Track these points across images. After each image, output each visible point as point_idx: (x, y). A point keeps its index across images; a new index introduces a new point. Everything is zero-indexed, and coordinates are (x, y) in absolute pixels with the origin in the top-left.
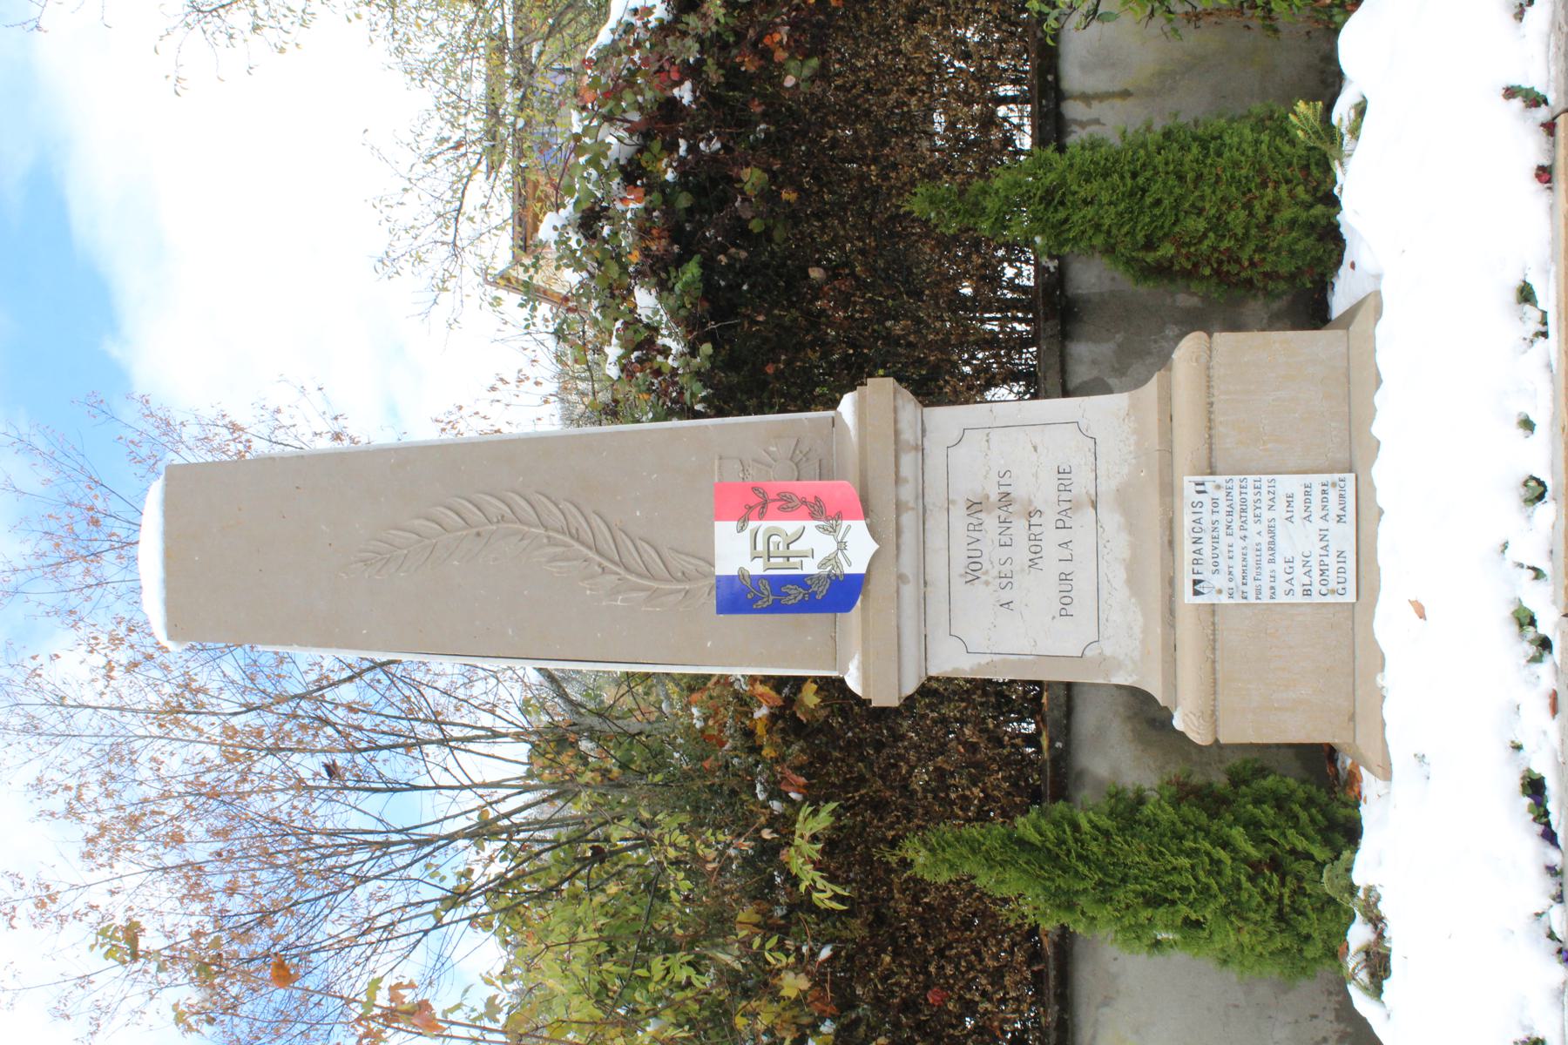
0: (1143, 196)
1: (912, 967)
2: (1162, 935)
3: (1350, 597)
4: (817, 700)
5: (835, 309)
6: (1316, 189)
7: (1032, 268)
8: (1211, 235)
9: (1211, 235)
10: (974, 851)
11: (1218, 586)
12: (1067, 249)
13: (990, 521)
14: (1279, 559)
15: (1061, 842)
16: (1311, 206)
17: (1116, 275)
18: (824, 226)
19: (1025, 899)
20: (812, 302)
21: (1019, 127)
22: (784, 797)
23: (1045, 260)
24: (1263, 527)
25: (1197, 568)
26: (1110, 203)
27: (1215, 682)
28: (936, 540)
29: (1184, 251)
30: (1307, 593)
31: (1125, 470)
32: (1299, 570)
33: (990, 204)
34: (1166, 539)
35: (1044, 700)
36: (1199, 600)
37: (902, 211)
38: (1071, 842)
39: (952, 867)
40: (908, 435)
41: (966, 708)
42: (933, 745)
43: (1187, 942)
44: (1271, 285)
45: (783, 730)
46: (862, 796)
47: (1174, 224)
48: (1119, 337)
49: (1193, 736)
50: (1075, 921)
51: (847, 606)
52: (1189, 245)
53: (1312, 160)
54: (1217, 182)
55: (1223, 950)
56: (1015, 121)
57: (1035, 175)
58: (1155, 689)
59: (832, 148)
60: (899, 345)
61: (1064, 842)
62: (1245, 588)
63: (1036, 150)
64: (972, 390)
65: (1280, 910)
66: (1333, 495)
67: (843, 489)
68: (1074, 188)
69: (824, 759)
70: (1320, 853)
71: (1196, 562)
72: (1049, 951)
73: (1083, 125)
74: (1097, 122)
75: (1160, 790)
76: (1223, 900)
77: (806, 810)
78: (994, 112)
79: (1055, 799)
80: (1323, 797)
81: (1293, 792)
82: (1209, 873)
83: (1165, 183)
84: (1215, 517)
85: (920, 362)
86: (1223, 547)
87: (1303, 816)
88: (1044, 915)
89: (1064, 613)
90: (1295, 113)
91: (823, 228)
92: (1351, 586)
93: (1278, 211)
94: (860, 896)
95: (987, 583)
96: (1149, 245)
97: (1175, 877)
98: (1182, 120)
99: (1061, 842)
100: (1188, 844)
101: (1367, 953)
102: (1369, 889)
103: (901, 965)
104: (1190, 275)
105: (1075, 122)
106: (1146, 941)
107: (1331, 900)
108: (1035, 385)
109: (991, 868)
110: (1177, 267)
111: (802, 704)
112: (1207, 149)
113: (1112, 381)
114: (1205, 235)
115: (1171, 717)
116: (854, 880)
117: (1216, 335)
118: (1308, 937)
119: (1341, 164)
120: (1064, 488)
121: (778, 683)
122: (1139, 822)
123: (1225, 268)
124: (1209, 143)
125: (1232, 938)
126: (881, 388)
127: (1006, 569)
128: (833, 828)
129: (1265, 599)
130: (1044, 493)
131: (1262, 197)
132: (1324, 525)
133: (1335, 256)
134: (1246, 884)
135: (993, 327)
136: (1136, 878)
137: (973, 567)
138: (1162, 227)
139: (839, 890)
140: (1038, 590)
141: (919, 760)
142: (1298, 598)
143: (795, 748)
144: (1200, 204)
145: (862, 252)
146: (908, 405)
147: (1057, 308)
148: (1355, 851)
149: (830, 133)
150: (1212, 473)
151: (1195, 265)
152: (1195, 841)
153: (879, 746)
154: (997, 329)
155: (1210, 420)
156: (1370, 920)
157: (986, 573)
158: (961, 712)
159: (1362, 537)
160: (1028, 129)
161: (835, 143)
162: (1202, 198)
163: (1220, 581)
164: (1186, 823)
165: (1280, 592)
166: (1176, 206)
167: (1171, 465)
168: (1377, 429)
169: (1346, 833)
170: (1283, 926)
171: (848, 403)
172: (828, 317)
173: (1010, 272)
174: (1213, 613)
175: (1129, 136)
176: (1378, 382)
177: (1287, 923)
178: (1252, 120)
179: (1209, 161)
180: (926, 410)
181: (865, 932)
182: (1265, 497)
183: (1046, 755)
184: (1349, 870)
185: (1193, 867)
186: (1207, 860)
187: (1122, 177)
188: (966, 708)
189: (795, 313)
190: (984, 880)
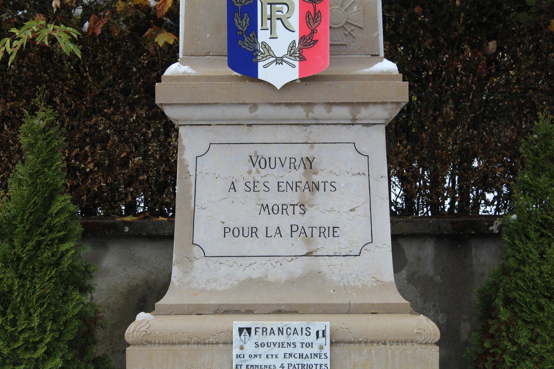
0: (546, 297)
4: (161, 44)
5: (464, 61)
7: (493, 213)
8: (515, 348)
9: (515, 348)
10: (43, 162)
11: (245, 346)
12: (506, 238)
13: (297, 175)
15: (51, 229)
18: (529, 53)
20: (469, 43)
22: (85, 17)
23: (498, 222)
25: (260, 330)
26: (541, 272)
27: (173, 344)
28: (283, 134)
29: (503, 327)
31: (335, 278)
34: (283, 308)
35: (161, 218)
36: (236, 332)
37: (539, 113)
38: (51, 236)
39: (31, 145)
40: (364, 113)
41: (155, 159)
42: (126, 134)
45: (137, 17)
46: (87, 78)
47: (524, 320)
48: (438, 278)
49: (132, 327)
51: (232, 65)
52: (508, 331)
58: (168, 300)
60: (435, 110)
61: (51, 231)
64: (400, 162)
67: (325, 65)
69: (116, 49)
71: (264, 330)
77: (75, 33)
79: (84, 225)
82: (26, 341)
84: (298, 345)
85: (421, 128)
86: (275, 350)
91: (527, 52)
94: (8, 76)
95: (250, 172)
96: (508, 301)
97: (23, 315)
99: (51, 229)
100: (49, 325)
104: (485, 333)
108: (400, 216)
109: (31, 175)
110: (490, 322)
111: (159, 32)
113: (404, 273)
114: (515, 344)
115: (146, 312)
116: (21, 72)
120: (322, 231)
121: (174, 14)
122: (66, 289)
126: (401, 92)
127: (260, 187)
128: (62, 54)
130: (318, 217)
136: (23, 286)
137: (263, 162)
138: (522, 311)
139: (12, 58)
141: (115, 122)
143: (124, 27)
144: (539, 340)
145: (508, 82)
146: (385, 114)
147: (462, 232)
150: (331, 343)
151: (492, 336)
152: (52, 331)
153: (126, 92)
154: (446, 185)
155: (372, 342)
157: (258, 172)
158: (152, 155)
162: (544, 342)
163: (250, 348)
164: (66, 323)
166: (538, 323)
171: (389, 66)
172: (458, 55)
173: (490, 197)
180: (383, 127)
183: (119, 219)
185: (32, 329)
188: (155, 159)
189: (461, 30)
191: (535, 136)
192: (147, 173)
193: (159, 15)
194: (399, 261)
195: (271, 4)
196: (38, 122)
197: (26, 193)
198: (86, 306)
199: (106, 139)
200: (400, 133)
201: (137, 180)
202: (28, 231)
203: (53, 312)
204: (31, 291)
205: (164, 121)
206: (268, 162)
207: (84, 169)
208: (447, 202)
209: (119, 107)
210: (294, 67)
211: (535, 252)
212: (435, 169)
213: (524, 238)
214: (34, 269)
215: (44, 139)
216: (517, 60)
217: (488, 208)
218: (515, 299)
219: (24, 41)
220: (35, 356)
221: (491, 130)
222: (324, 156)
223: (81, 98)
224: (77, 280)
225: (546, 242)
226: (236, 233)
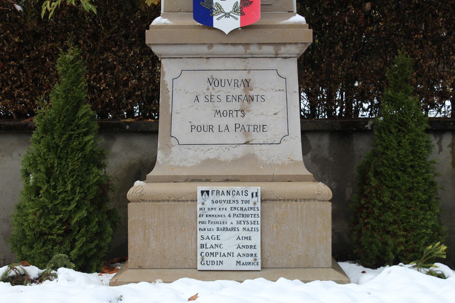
0: (401, 170)
1: (13, 53)
2: (31, 177)
3: (200, 267)
5: (349, 16)
6: (402, 255)
7: (367, 116)
8: (381, 204)
9: (381, 204)
10: (73, 83)
11: (205, 203)
12: (376, 133)
13: (239, 91)
14: (219, 233)
15: (78, 126)
16: (394, 253)
17: (362, 158)
19: (48, 109)
21: (439, 111)
23: (371, 123)
24: (235, 225)
25: (215, 192)
26: (398, 154)
27: (159, 201)
28: (230, 64)
29: (373, 190)
30: (202, 246)
31: (264, 159)
32: (213, 242)
33: (400, 94)
34: (230, 178)
35: (150, 120)
36: (199, 194)
37: (399, 51)
38: (78, 131)
39: (64, 72)
40: (283, 50)
41: (146, 81)
42: (127, 64)
43: (28, 188)
44: (355, 233)
46: (100, 27)
47: (387, 186)
48: (331, 159)
49: (131, 190)
50: (38, 133)
51: (196, 18)
52: (376, 193)
53: (417, 254)
54: (407, 207)
55: (25, 206)
56: (443, 109)
57: (414, 117)
58: (154, 173)
59: (433, 15)
60: (330, 49)
61: (78, 128)
62: (205, 216)
63: (426, 119)
65: (45, 234)
66: (250, 259)
67: (257, 18)
68: (407, 137)
70: (74, 252)
71: (218, 192)
72: (23, 122)
73: (439, 143)
74: (441, 150)
75: (106, 176)
76: (50, 206)
78: (447, 99)
79: (100, 124)
80: (102, 255)
81: (104, 240)
82: (63, 199)
83: (408, 182)
86: (225, 205)
87: (92, 245)
88: (41, 118)
89: (192, 128)
90: (440, 244)
91: (391, 10)
92: (205, 267)
93: (392, 237)
94: (48, 26)
95: (208, 89)
96: (377, 174)
97: (61, 182)
98: (440, 191)
99: (78, 126)
100: (78, 189)
101: (24, 275)
102: (56, 276)
103: (13, 47)
104: (362, 194)
105: (441, 139)
106: (28, 168)
107: (50, 258)
109: (64, 91)
110: (365, 187)
112: (425, 203)
113: (309, 155)
114: (381, 201)
115: (141, 180)
116: (57, 23)
117: (331, 204)
118: (32, 248)
119: (414, 267)
120: (256, 128)
122: (88, 166)
123: (364, 211)
124: (427, 204)
125: (31, 211)
126: (307, 36)
127: (215, 99)
128: (84, 12)
129: (199, 226)
131: (399, 229)
132: (236, 255)
133: (369, 264)
134: (58, 218)
135: (338, 96)
136: (60, 164)
137: (216, 82)
138: (386, 180)
139: (51, 14)
140: (204, 115)
141: (120, 57)
142: (200, 242)
144: (396, 199)
145: (378, 30)
147: (347, 129)
148: (75, 269)
149: (440, 14)
150: (262, 201)
151: (366, 196)
152: (79, 193)
153: (126, 37)
154: (337, 98)
155: (288, 200)
156: (40, 276)
157: (213, 89)
159: (230, 273)
160: (439, 115)
161: (435, 16)
162: (400, 200)
163: (208, 204)
164: (88, 188)
165: (202, 233)
167: (266, 181)
168: (282, 280)
169: (84, 266)
170: (38, 235)
171: (299, 19)
172: (345, 12)
173: (366, 106)
174: (192, 201)
175: (432, 165)
176: (305, 282)
177: (39, 238)
178: (438, 225)
179: (418, 203)
180: (296, 59)
181: (30, 29)
182: (250, 226)
184: (65, 266)
185: (67, 191)
186: (70, 198)
187: (411, 161)
190: (58, 88)
191: (396, 65)
196: (69, 57)
197: (61, 103)
201: (134, 95)
202: (63, 128)
203: (80, 181)
204: (66, 167)
205: (152, 56)
206: (220, 82)
207: (100, 87)
209: (122, 47)
210: (237, 19)
211: (395, 141)
212: (330, 88)
213: (387, 133)
214: (67, 152)
215: (73, 68)
217: (365, 113)
218: (381, 172)
220: (69, 209)
222: (257, 79)
224: (96, 160)
225: (402, 135)
226: (199, 129)
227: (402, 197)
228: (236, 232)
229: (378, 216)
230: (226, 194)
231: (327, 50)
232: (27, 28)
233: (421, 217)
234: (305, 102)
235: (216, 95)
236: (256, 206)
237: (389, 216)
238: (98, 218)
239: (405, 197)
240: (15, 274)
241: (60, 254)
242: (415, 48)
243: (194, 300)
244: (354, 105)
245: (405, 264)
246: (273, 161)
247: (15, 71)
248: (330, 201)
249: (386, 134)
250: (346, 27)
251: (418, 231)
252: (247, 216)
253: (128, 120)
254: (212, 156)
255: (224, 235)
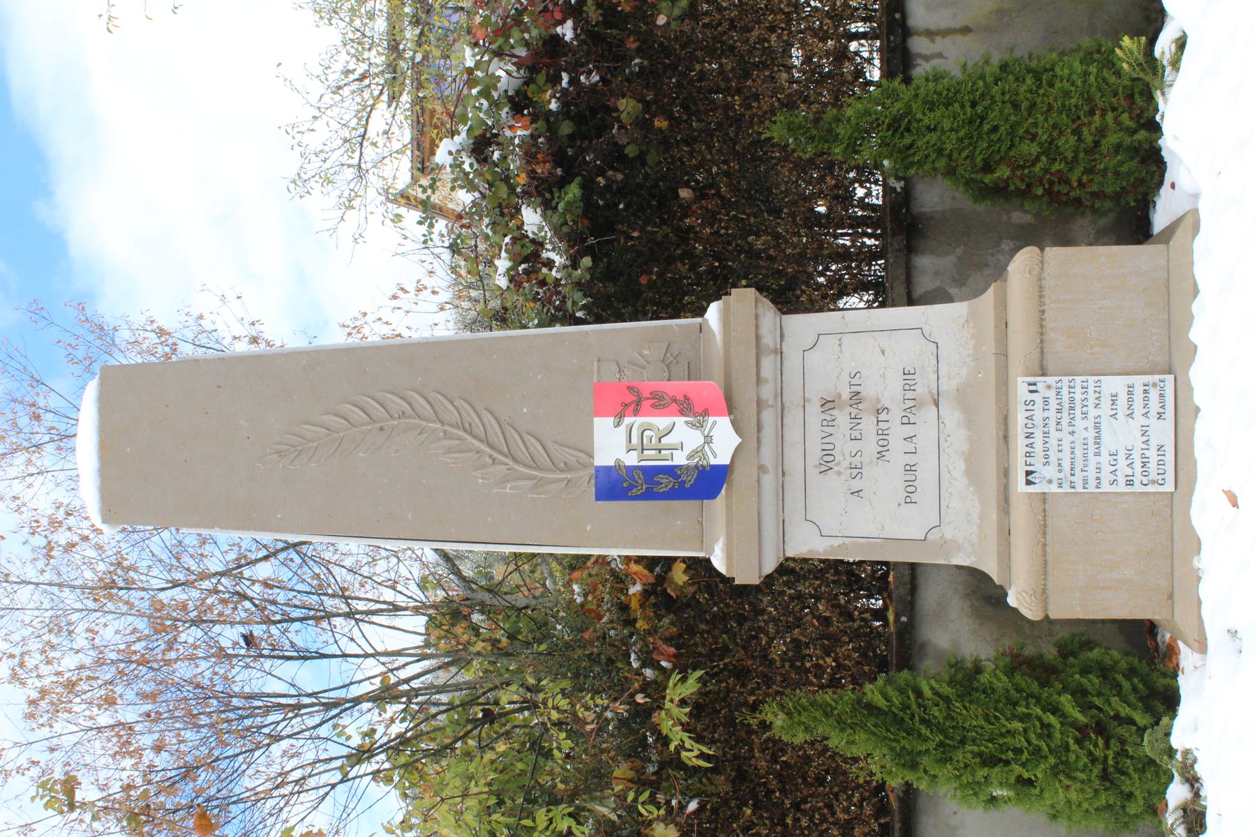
0: (981, 123)
2: (998, 792)
3: (1169, 487)
4: (685, 578)
6: (1139, 116)
7: (880, 188)
8: (1044, 158)
9: (1044, 158)
10: (826, 715)
11: (1048, 477)
12: (912, 171)
13: (842, 418)
15: (905, 707)
16: (1135, 132)
18: (693, 151)
19: (874, 759)
20: (681, 219)
21: (869, 61)
22: (656, 666)
23: (892, 182)
24: (1090, 424)
25: (1029, 460)
26: (952, 130)
27: (1045, 562)
28: (793, 435)
29: (1019, 173)
30: (1130, 483)
31: (964, 372)
32: (1122, 463)
34: (1001, 434)
35: (891, 579)
36: (1031, 489)
37: (763, 137)
38: (914, 707)
40: (768, 340)
41: (820, 586)
42: (791, 619)
44: (1098, 204)
45: (654, 605)
46: (726, 665)
47: (1010, 148)
48: (959, 251)
50: (918, 779)
51: (713, 494)
52: (1023, 167)
53: (1137, 90)
54: (1049, 110)
55: (1052, 806)
56: (866, 55)
59: (700, 80)
61: (909, 707)
64: (824, 300)
65: (1105, 770)
66: (1154, 394)
67: (710, 388)
68: (919, 116)
69: (692, 631)
70: (1141, 718)
71: (1028, 455)
72: (895, 805)
73: (927, 58)
74: (940, 55)
77: (676, 677)
78: (846, 47)
79: (900, 668)
81: (1117, 663)
82: (1040, 736)
83: (1001, 112)
84: (1046, 414)
85: (780, 274)
86: (1053, 441)
87: (1126, 685)
90: (1120, 47)
91: (691, 153)
92: (1170, 476)
93: (1104, 136)
95: (839, 473)
96: (987, 168)
97: (1009, 740)
98: (1018, 54)
99: (905, 707)
100: (1021, 710)
101: (1185, 810)
102: (1187, 752)
103: (761, 817)
104: (1025, 194)
107: (1152, 762)
108: (883, 295)
109: (842, 730)
110: (1012, 188)
111: (672, 581)
112: (1040, 80)
113: (953, 291)
114: (1038, 159)
115: (1006, 595)
116: (719, 740)
118: (1130, 796)
119: (1163, 94)
121: (651, 562)
122: (977, 690)
124: (1042, 75)
126: (744, 298)
128: (699, 693)
129: (1092, 488)
130: (890, 391)
131: (1090, 123)
132: (1145, 421)
134: (1074, 747)
137: (826, 458)
138: (999, 151)
140: (885, 481)
141: (777, 632)
142: (1121, 488)
143: (666, 621)
144: (1033, 131)
145: (727, 174)
146: (768, 312)
148: (1173, 717)
149: (698, 67)
150: (1043, 375)
151: (1029, 186)
152: (1027, 707)
153: (741, 620)
154: (848, 243)
155: (1042, 326)
156: (1187, 780)
157: (838, 464)
158: (815, 589)
159: (1180, 432)
160: (877, 62)
161: (702, 76)
162: (1035, 125)
163: (1050, 472)
164: (1019, 690)
168: (1195, 335)
169: (1167, 701)
170: (1108, 784)
171: (714, 311)
172: (696, 233)
173: (860, 192)
175: (969, 69)
176: (1196, 292)
177: (1111, 781)
178: (1081, 54)
179: (1042, 91)
180: (784, 317)
181: (728, 788)
182: (1092, 396)
183: (892, 628)
184: (1168, 734)
185: (1025, 730)
186: (1037, 723)
187: (963, 106)
189: (666, 229)
190: (836, 741)
191: (791, 141)
192: (836, 595)
193: (652, 580)
194: (938, 296)
195: (643, 450)
196: (779, 720)
197: (864, 736)
198: (997, 666)
199: (797, 644)
200: (790, 295)
201: (845, 607)
202: (909, 734)
203: (1005, 705)
204: (980, 731)
205: (776, 575)
206: (827, 453)
207: (832, 668)
208: (868, 242)
209: (759, 627)
210: (715, 423)
211: (927, 137)
212: (830, 256)
213: (912, 151)
214: (953, 727)
215: (799, 714)
216: (701, 165)
217: (874, 193)
218: (984, 160)
219: (685, 736)
220: (1058, 726)
221: (782, 192)
222: (819, 387)
223: (749, 671)
224: (966, 678)
225: (915, 125)
226: (912, 489)
227: (1030, 121)
228: (1102, 420)
229: (1067, 163)
230: (1031, 441)
231: (762, 263)
232: (727, 793)
233: (1066, 85)
234: (853, 301)
235: (849, 459)
236: (1054, 385)
237: (1067, 143)
238: (1074, 673)
239: (1029, 115)
240: (1182, 826)
241: (1145, 743)
242: (759, 108)
243: (1235, 497)
244: (860, 213)
245: (1157, 110)
246: (969, 355)
247: (805, 816)
248: (1042, 250)
249: (914, 154)
250: (722, 231)
251: (1093, 89)
252: (1072, 400)
253: (891, 617)
254: (962, 466)
255: (1108, 442)
